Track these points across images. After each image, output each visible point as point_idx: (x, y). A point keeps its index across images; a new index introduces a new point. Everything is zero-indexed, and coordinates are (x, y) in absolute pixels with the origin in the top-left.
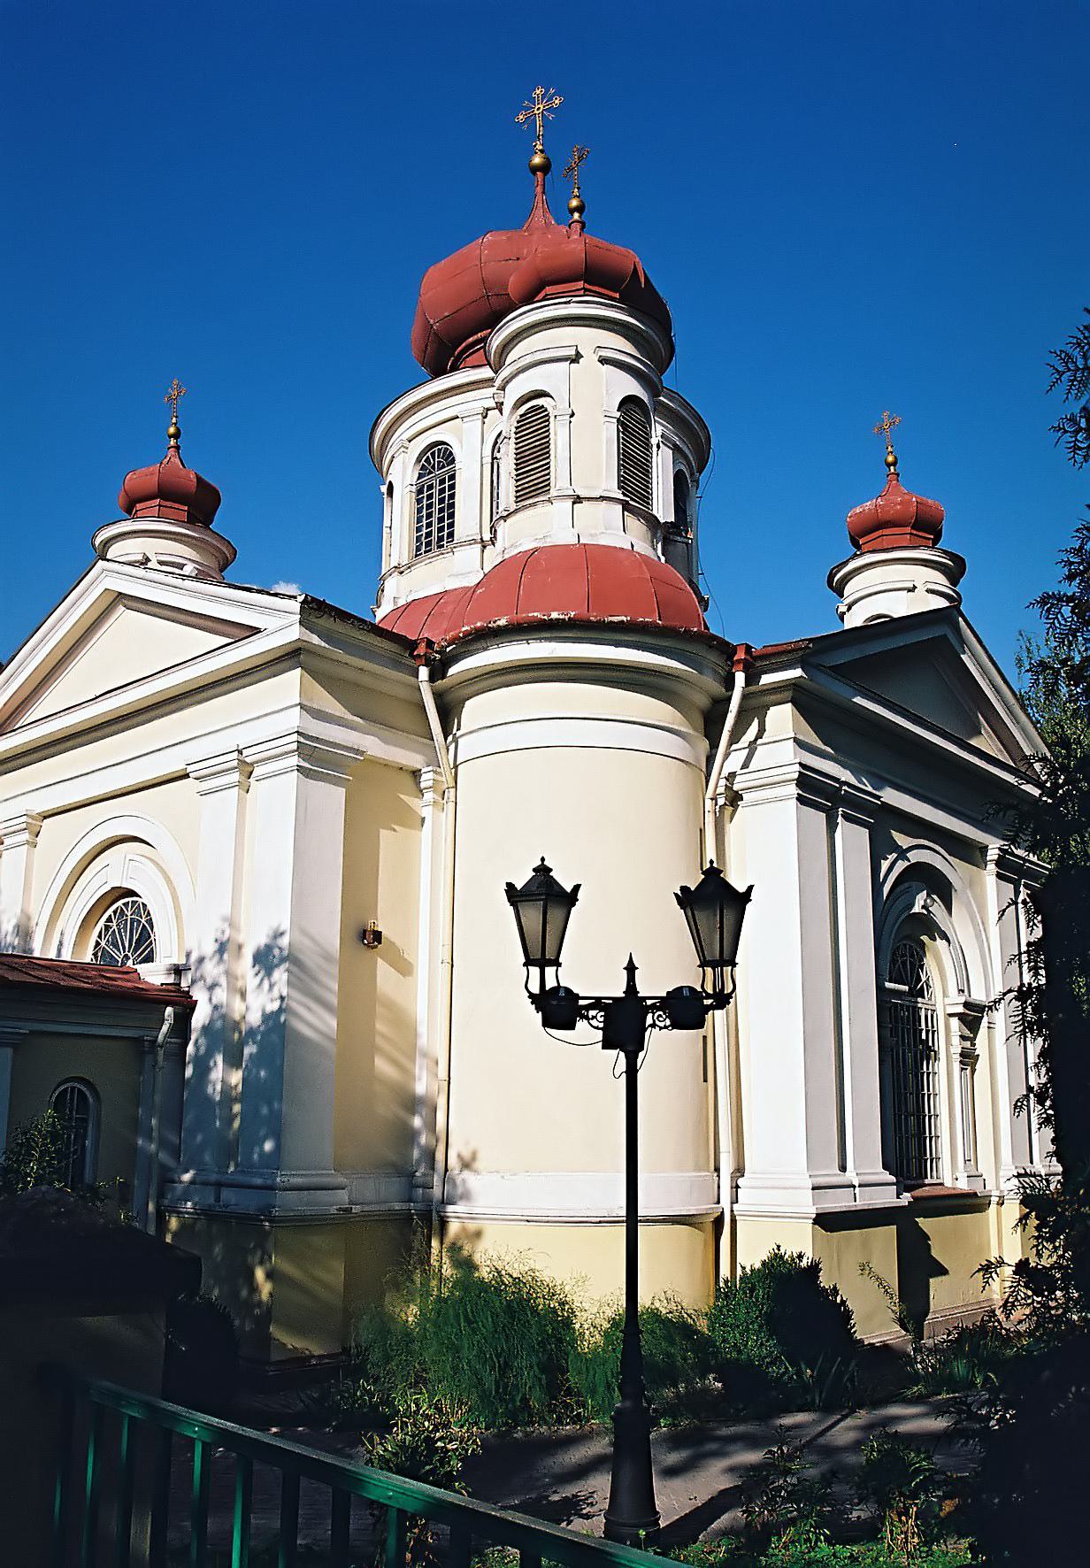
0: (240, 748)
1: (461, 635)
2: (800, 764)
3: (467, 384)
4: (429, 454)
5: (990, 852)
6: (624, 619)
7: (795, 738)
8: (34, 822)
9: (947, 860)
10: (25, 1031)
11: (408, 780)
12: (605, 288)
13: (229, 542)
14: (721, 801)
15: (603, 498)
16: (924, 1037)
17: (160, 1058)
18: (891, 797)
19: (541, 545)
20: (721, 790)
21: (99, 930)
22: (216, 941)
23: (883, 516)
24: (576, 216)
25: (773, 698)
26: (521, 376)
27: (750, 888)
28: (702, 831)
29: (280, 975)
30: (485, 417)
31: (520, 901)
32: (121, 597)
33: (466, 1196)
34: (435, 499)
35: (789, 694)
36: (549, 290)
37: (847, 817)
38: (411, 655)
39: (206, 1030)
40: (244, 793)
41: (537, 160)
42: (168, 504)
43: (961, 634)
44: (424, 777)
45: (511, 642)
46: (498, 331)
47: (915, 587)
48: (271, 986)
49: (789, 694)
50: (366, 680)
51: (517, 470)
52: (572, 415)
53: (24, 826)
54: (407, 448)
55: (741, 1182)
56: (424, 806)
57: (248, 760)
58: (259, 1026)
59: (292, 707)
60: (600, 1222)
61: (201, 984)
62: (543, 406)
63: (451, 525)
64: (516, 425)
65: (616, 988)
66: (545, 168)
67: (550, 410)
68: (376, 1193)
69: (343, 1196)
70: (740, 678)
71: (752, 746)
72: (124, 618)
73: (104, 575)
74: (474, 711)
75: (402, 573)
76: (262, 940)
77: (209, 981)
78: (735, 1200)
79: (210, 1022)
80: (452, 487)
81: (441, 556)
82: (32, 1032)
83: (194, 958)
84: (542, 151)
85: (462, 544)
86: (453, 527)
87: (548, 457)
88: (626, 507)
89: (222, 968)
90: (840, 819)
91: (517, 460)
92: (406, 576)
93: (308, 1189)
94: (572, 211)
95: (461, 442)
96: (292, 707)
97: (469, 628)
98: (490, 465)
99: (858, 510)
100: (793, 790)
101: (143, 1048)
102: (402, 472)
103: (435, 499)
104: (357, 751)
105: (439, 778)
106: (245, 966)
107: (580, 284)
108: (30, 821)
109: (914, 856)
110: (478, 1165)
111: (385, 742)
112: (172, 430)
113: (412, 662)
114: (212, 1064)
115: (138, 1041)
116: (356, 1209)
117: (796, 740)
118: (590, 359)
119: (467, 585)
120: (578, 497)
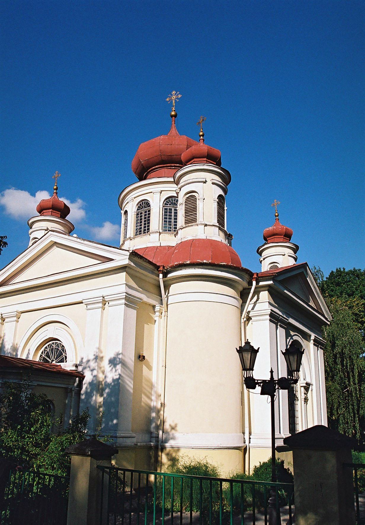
0: (104, 296)
1: (174, 265)
2: (271, 310)
3: (156, 182)
4: (144, 201)
5: (312, 337)
6: (225, 264)
7: (126, 284)
8: (19, 314)
9: (301, 339)
10: (35, 384)
11: (151, 308)
12: (212, 161)
13: (73, 226)
14: (245, 319)
15: (213, 225)
16: (295, 393)
17: (73, 394)
18: (291, 321)
19: (194, 238)
20: (246, 316)
21: (42, 351)
22: (94, 355)
23: (275, 232)
24: (202, 137)
25: (262, 289)
26: (187, 185)
27: (259, 348)
28: (241, 328)
29: (119, 367)
30: (161, 193)
31: (243, 352)
32: (55, 244)
33: (173, 438)
34: (143, 217)
35: (267, 288)
36: (195, 160)
37: (281, 326)
38: (157, 270)
39: (91, 384)
40: (103, 310)
41: (173, 113)
42: (55, 211)
43: (307, 272)
44: (156, 308)
45: (189, 268)
46: (180, 171)
47: (285, 254)
48: (116, 371)
49: (267, 288)
50: (143, 277)
51: (185, 214)
52: (204, 199)
53: (15, 315)
54: (133, 200)
55: (251, 437)
56: (156, 317)
57: (106, 300)
58: (111, 383)
59: (122, 284)
60: (215, 449)
61: (88, 369)
62: (194, 196)
63: (149, 226)
64: (185, 200)
65: (268, 378)
66: (175, 116)
67: (197, 197)
68: (139, 439)
69: (134, 440)
70: (254, 283)
71: (255, 303)
72: (55, 249)
73: (51, 236)
74: (173, 288)
75: (131, 240)
76: (112, 355)
77: (92, 368)
78: (250, 443)
79: (92, 381)
80: (149, 214)
81: (146, 236)
82: (38, 385)
83: (84, 360)
84: (174, 111)
85: (153, 233)
86: (149, 227)
87: (196, 211)
88: (220, 229)
89: (96, 364)
90: (279, 326)
91: (185, 209)
92: (133, 241)
93: (126, 438)
94: (200, 136)
95: (153, 200)
96: (122, 284)
97: (177, 263)
98: (162, 209)
99: (267, 229)
100: (268, 317)
101: (67, 391)
102: (131, 207)
103: (143, 217)
104: (141, 299)
105: (161, 308)
106: (105, 364)
107: (205, 159)
108: (17, 314)
109: (295, 338)
110: (178, 428)
111: (148, 297)
112: (55, 187)
113: (156, 272)
114: (92, 395)
115: (66, 389)
116: (139, 444)
117: (126, 284)
118: (209, 183)
119: (154, 246)
120: (206, 224)
